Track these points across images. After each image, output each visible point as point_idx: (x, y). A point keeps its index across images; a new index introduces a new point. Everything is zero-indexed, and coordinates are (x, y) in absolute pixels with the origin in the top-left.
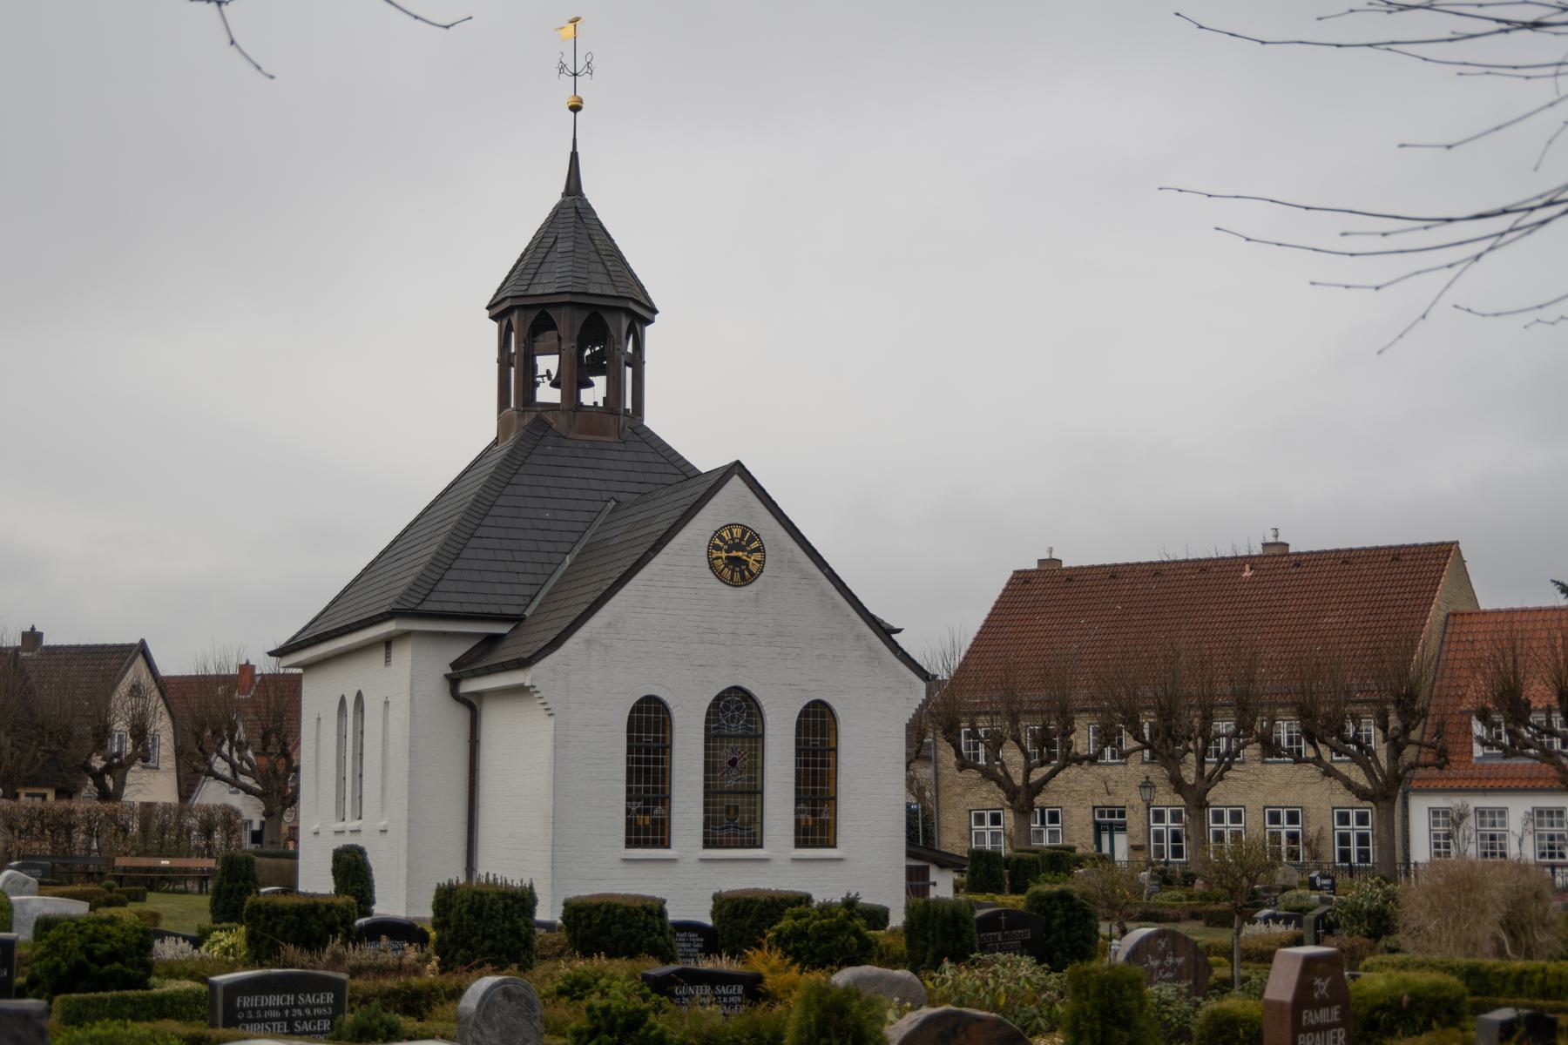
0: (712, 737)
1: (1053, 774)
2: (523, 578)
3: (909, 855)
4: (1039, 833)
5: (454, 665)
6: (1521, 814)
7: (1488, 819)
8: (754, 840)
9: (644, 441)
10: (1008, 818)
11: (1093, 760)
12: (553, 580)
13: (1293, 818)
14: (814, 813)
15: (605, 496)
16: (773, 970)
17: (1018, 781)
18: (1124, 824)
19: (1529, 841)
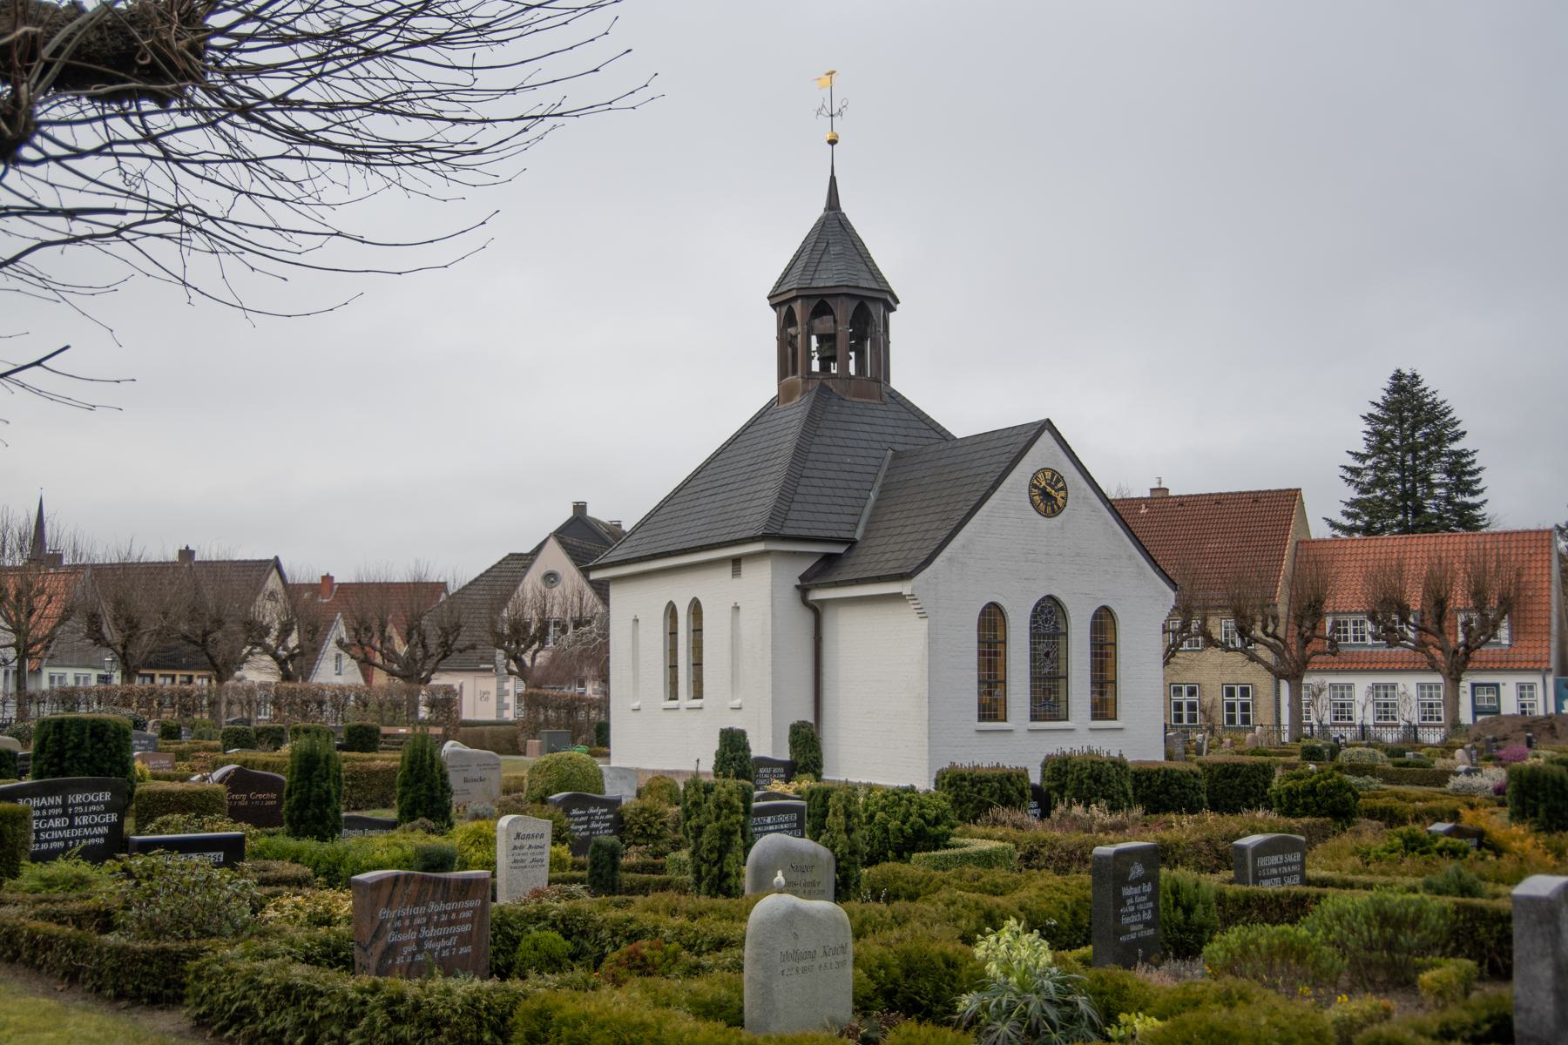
0: (1035, 636)
2: (846, 510)
5: (802, 578)
6: (1365, 688)
7: (1382, 692)
9: (899, 403)
13: (1192, 692)
15: (885, 446)
19: (1370, 708)
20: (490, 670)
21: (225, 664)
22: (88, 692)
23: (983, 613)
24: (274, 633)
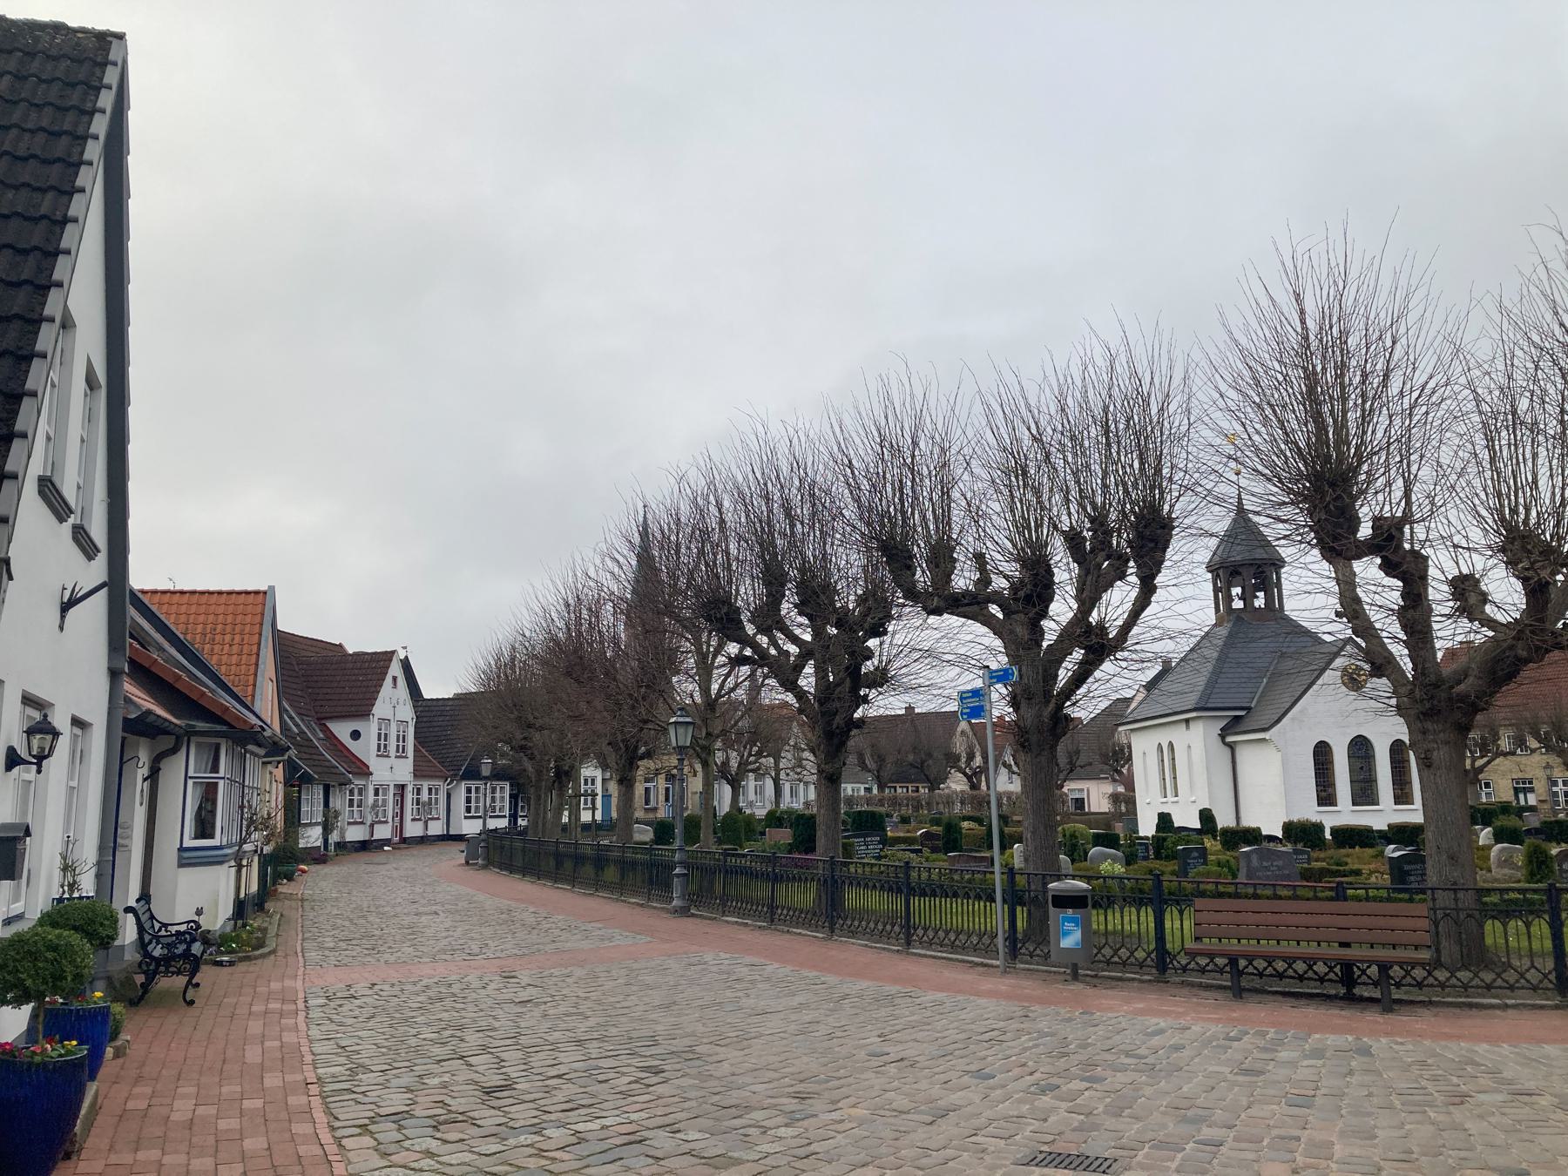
1: (1489, 762)
11: (1513, 753)
12: (1261, 689)
14: (1402, 790)
20: (1107, 778)
21: (935, 779)
22: (862, 798)
23: (1316, 746)
24: (964, 760)
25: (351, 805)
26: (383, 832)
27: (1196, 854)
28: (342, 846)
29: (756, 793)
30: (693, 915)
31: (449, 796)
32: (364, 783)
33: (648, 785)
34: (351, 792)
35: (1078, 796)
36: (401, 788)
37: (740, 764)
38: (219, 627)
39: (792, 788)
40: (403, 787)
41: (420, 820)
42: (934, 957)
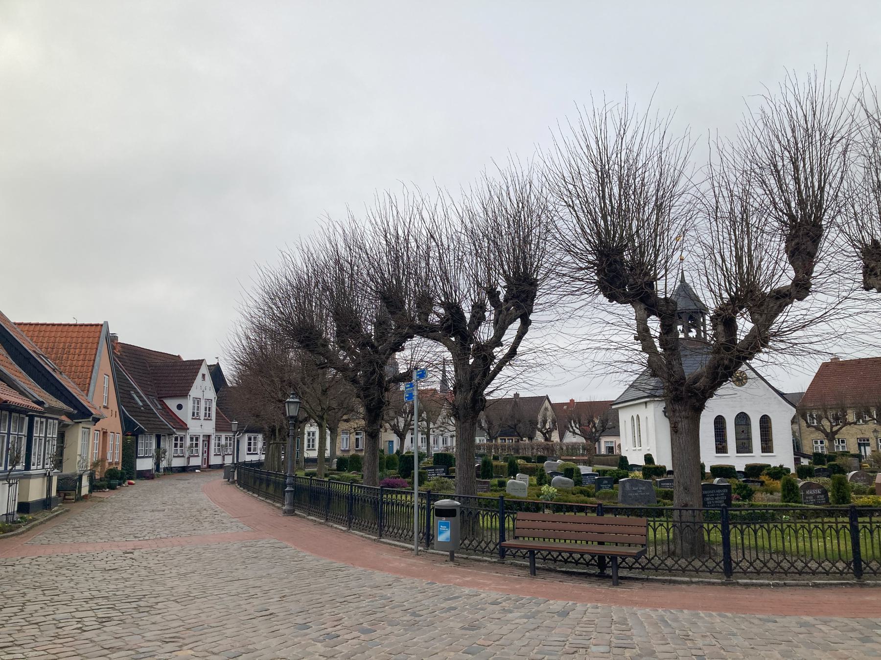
1: (841, 428)
3: (794, 454)
4: (838, 447)
8: (750, 451)
10: (826, 442)
11: (855, 423)
14: (766, 444)
16: (767, 480)
17: (829, 431)
18: (869, 443)
25: (176, 445)
26: (195, 462)
27: (606, 482)
28: (170, 470)
29: (422, 442)
30: (296, 515)
31: (238, 441)
32: (184, 434)
33: (357, 436)
34: (176, 439)
35: (610, 445)
36: (208, 437)
37: (405, 425)
38: (73, 345)
39: (434, 439)
40: (209, 436)
41: (220, 455)
42: (390, 544)
